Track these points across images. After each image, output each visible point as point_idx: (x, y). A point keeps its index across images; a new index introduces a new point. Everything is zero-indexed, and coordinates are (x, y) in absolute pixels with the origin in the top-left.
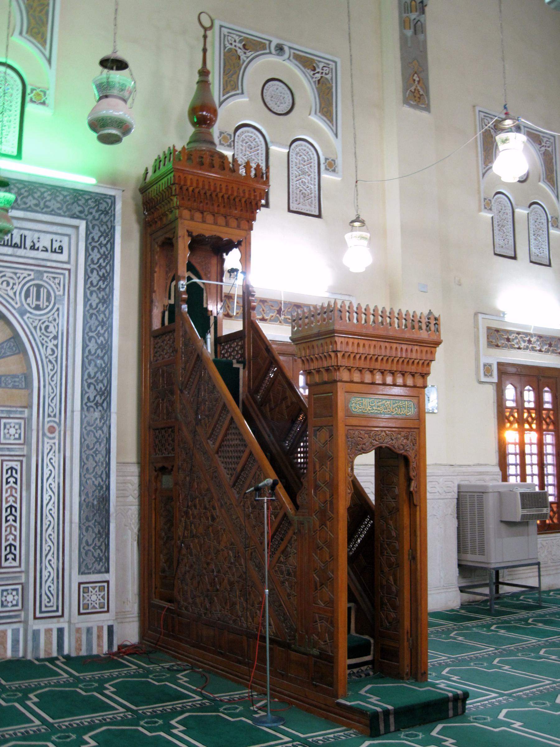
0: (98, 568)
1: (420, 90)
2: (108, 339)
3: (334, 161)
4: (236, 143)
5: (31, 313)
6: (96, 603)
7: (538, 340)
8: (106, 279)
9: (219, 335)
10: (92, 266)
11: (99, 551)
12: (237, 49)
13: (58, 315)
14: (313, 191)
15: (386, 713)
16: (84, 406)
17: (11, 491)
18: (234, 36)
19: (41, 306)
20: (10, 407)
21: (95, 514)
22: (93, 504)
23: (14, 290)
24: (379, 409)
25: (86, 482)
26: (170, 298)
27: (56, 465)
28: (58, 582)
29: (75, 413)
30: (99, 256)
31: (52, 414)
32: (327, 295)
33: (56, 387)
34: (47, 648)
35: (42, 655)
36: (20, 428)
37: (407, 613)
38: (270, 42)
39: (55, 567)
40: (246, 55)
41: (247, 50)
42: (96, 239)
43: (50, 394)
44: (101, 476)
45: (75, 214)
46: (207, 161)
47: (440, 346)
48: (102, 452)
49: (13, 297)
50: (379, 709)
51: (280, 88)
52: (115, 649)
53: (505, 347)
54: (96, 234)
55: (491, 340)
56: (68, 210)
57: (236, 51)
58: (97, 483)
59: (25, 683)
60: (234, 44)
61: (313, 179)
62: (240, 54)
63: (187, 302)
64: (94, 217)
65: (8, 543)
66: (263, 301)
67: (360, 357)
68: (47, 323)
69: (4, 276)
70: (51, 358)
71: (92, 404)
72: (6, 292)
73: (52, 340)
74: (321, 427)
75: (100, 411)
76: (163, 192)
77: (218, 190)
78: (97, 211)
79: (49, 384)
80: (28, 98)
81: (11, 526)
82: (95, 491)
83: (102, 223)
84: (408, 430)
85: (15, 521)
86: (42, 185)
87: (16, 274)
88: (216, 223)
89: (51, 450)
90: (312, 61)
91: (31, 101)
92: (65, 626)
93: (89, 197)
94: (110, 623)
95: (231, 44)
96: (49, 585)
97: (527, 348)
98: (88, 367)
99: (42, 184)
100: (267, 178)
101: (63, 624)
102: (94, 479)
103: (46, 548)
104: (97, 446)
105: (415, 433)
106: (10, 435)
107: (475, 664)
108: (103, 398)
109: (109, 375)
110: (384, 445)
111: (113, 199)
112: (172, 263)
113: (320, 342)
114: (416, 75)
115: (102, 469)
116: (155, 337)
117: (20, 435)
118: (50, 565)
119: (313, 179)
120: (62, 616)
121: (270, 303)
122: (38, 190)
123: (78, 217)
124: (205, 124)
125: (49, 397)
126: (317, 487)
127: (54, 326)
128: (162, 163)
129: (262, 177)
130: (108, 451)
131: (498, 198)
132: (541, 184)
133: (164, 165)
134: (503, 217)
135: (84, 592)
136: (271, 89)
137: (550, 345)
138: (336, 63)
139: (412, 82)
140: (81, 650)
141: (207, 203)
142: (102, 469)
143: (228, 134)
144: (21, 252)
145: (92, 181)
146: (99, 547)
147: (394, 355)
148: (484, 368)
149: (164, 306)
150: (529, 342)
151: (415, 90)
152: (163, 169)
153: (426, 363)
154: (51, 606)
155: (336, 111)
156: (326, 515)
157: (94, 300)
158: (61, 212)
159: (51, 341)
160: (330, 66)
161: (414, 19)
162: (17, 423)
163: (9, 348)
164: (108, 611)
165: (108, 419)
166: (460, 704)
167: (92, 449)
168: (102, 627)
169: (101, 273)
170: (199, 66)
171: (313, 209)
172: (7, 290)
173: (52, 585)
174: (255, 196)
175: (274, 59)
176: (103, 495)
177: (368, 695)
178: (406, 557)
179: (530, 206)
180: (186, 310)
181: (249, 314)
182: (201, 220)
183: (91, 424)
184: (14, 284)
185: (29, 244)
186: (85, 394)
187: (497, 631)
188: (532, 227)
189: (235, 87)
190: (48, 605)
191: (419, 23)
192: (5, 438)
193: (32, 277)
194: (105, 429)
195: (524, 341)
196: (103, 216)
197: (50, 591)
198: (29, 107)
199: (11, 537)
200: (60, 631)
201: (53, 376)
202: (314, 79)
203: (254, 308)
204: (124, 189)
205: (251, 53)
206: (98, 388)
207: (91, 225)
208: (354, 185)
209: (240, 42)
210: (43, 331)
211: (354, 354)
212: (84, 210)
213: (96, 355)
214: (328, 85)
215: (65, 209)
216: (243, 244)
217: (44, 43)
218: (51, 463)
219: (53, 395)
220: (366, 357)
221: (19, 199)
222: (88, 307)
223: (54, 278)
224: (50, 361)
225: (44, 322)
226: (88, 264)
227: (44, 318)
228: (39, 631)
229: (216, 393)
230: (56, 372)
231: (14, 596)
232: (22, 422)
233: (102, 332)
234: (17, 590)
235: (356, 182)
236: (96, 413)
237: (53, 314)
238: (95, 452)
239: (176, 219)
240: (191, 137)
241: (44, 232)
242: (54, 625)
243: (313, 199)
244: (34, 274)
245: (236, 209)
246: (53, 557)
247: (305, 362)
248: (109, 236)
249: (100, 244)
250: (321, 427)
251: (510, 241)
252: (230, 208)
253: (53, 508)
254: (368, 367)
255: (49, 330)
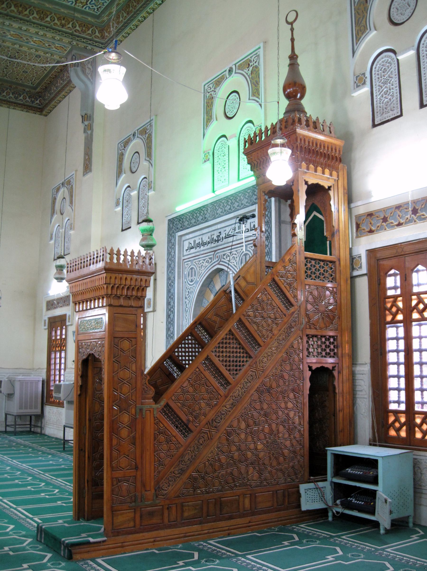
184: (236, 257)
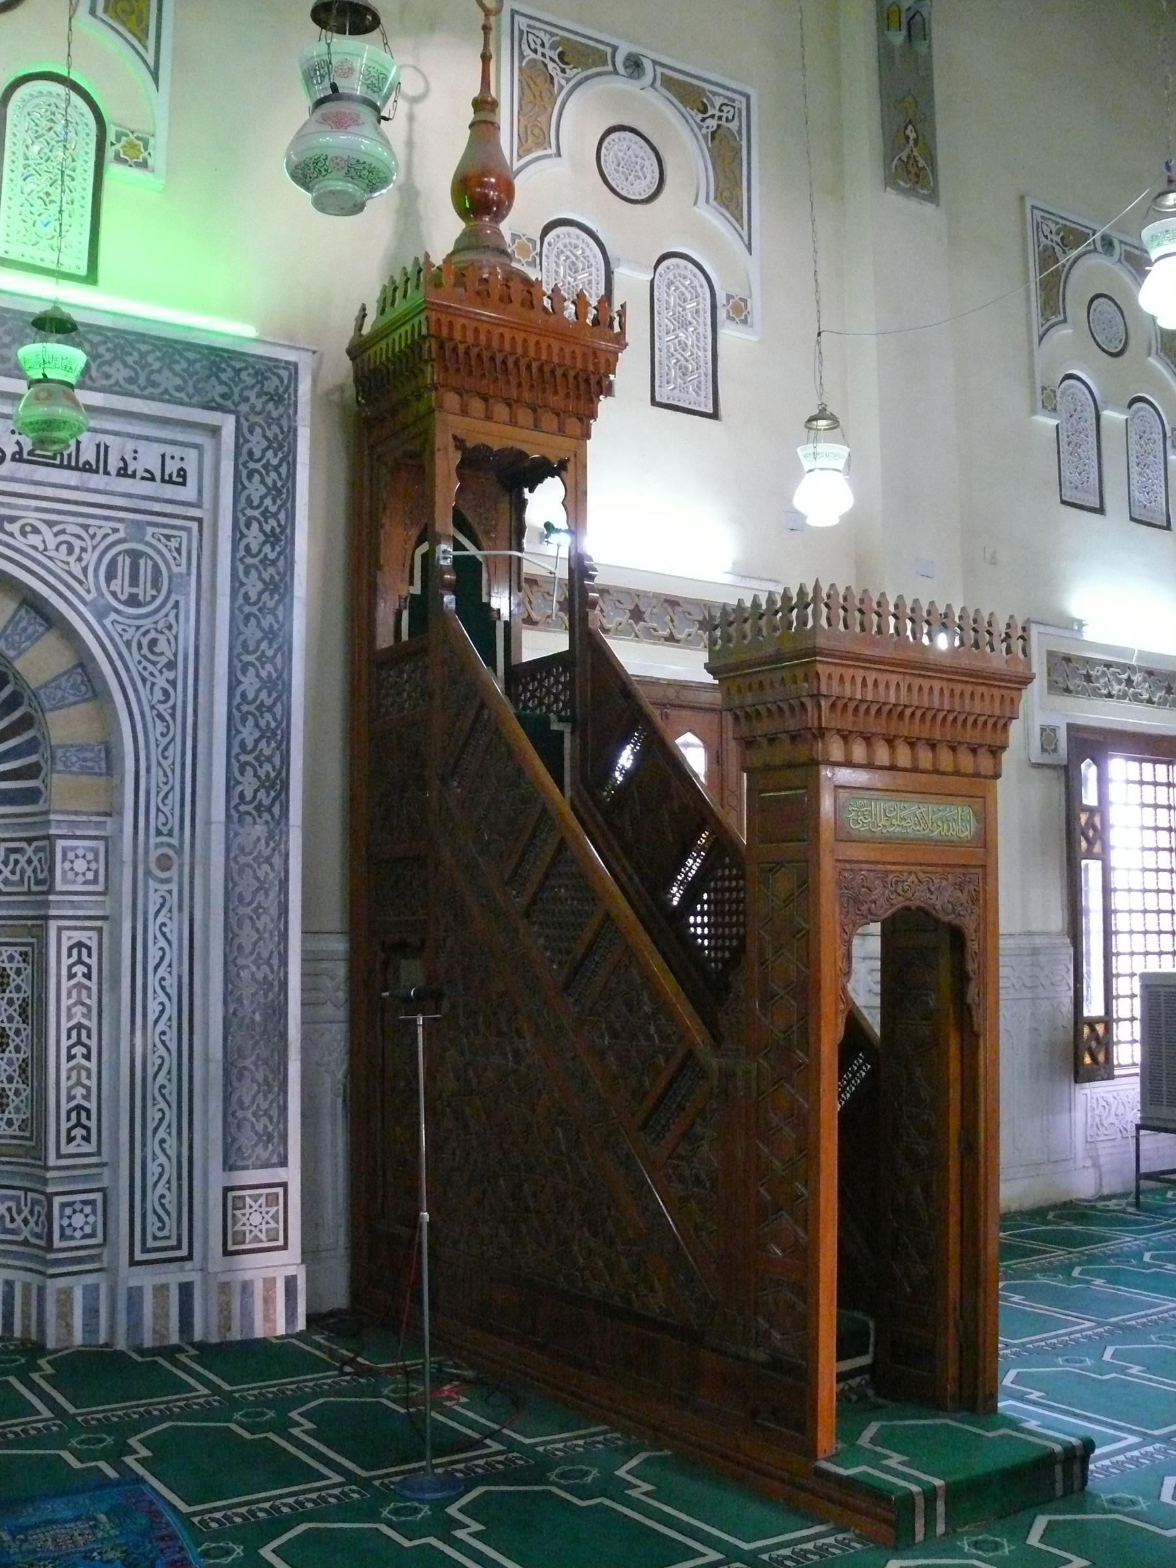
0: (265, 1155)
1: (919, 159)
2: (283, 669)
3: (745, 301)
4: (544, 258)
5: (118, 612)
6: (261, 1231)
7: (1145, 680)
8: (278, 540)
9: (514, 662)
10: (249, 512)
11: (264, 1120)
12: (547, 61)
13: (177, 616)
14: (702, 364)
15: (930, 1495)
16: (233, 812)
17: (79, 994)
18: (541, 34)
19: (141, 597)
20: (76, 813)
21: (257, 1043)
22: (253, 1021)
23: (84, 563)
24: (904, 823)
25: (238, 975)
26: (411, 583)
27: (174, 940)
28: (180, 1186)
29: (213, 827)
30: (263, 490)
31: (165, 830)
32: (728, 579)
33: (173, 771)
34: (158, 1325)
35: (148, 1343)
36: (96, 859)
37: (954, 1267)
38: (615, 49)
39: (173, 1153)
40: (567, 76)
41: (567, 64)
42: (258, 455)
43: (161, 785)
44: (268, 962)
45: (213, 400)
46: (496, 290)
47: (1029, 686)
48: (272, 911)
49: (83, 578)
50: (915, 1488)
51: (634, 146)
52: (301, 1325)
53: (1084, 692)
54: (257, 443)
55: (1055, 678)
56: (198, 391)
57: (545, 65)
58: (259, 976)
59: (115, 1410)
60: (540, 50)
61: (702, 339)
62: (554, 74)
63: (454, 589)
64: (253, 408)
65: (73, 1104)
66: (604, 591)
67: (868, 709)
68: (153, 634)
69: (63, 532)
70: (161, 707)
71: (250, 808)
72: (66, 567)
73: (164, 670)
74: (779, 864)
75: (267, 822)
76: (407, 351)
77: (520, 351)
78: (259, 396)
79: (159, 764)
80: (110, 153)
81: (79, 1067)
82: (256, 993)
83: (270, 420)
84: (961, 870)
85: (87, 1057)
86: (143, 337)
87: (86, 527)
88: (513, 422)
89: (162, 905)
90: (701, 92)
91: (118, 159)
92: (195, 1277)
93: (243, 365)
94: (291, 1271)
95: (535, 51)
96: (162, 1193)
97: (1124, 696)
98: (241, 728)
99: (144, 335)
100: (622, 326)
101: (190, 1273)
102: (254, 969)
103: (153, 1115)
104: (261, 896)
105: (976, 877)
106: (77, 874)
107: (1067, 1361)
108: (273, 794)
109: (284, 746)
110: (914, 904)
111: (292, 368)
112: (424, 503)
113: (780, 674)
114: (910, 127)
115: (271, 946)
116: (381, 666)
117: (96, 872)
118: (163, 1150)
119: (702, 339)
120: (190, 1257)
121: (615, 596)
122: (134, 348)
123: (220, 408)
124: (488, 211)
125: (158, 792)
126: (768, 998)
127: (168, 641)
128: (399, 294)
129: (611, 326)
130: (284, 909)
131: (1069, 387)
132: (1152, 360)
133: (405, 296)
134: (1080, 427)
135: (235, 1208)
136: (616, 147)
137: (1169, 690)
138: (748, 97)
139: (903, 141)
140: (230, 1329)
141: (496, 379)
142: (271, 946)
143: (529, 240)
144: (96, 480)
145: (250, 331)
146: (266, 1112)
147: (936, 705)
148: (1042, 735)
149: (400, 597)
150: (1129, 682)
151: (909, 157)
152: (401, 306)
153: (1001, 722)
154: (168, 1238)
155: (749, 199)
156: (792, 1057)
157: (253, 587)
158: (183, 395)
159: (161, 672)
160: (736, 104)
161: (909, 9)
162: (91, 849)
163: (72, 688)
164: (285, 1247)
165: (284, 839)
166: (1076, 1469)
167: (249, 904)
168: (274, 1279)
169: (267, 528)
170: (476, 91)
171: (702, 399)
172: (68, 563)
173: (166, 1193)
174: (596, 365)
175: (621, 84)
176: (273, 1001)
177: (879, 1449)
178: (954, 1146)
179: (1129, 406)
180: (453, 606)
181: (584, 618)
182: (482, 415)
183: (247, 851)
184: (83, 550)
185: (114, 464)
186: (235, 786)
187: (1088, 1282)
188: (1134, 448)
189: (543, 142)
190: (160, 1234)
191: (918, 17)
192: (65, 880)
193: (121, 535)
194: (277, 861)
195: (1120, 682)
196: (271, 405)
197: (163, 1205)
198: (113, 171)
199: (80, 1091)
200: (186, 1290)
201: (165, 749)
202: (704, 131)
203: (593, 604)
204: (316, 349)
205: (575, 71)
206: (262, 773)
207: (245, 425)
208: (814, 343)
209: (553, 47)
210: (145, 651)
211: (855, 703)
212: (232, 393)
213: (258, 702)
214: (733, 144)
215: (191, 390)
216: (570, 466)
217: (142, 36)
218: (164, 934)
219: (167, 788)
220: (879, 711)
221: (94, 366)
222: (240, 600)
223: (168, 537)
224: (160, 716)
225: (148, 631)
226: (240, 507)
227: (147, 623)
228: (140, 1289)
229: (524, 785)
230: (173, 739)
231: (86, 1216)
232: (101, 845)
233: (270, 653)
234: (92, 1203)
235: (819, 334)
236: (257, 827)
237: (167, 615)
238: (255, 911)
239: (431, 411)
240: (457, 242)
241: (147, 438)
242: (173, 1277)
243: (703, 378)
244: (126, 528)
245: (556, 393)
246: (169, 1134)
247: (743, 720)
248: (285, 449)
249: (264, 466)
250: (777, 863)
251: (1091, 477)
252: (544, 390)
253: (167, 1029)
254: (884, 731)
255: (157, 650)
